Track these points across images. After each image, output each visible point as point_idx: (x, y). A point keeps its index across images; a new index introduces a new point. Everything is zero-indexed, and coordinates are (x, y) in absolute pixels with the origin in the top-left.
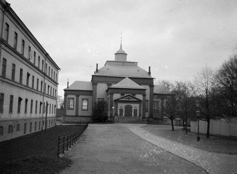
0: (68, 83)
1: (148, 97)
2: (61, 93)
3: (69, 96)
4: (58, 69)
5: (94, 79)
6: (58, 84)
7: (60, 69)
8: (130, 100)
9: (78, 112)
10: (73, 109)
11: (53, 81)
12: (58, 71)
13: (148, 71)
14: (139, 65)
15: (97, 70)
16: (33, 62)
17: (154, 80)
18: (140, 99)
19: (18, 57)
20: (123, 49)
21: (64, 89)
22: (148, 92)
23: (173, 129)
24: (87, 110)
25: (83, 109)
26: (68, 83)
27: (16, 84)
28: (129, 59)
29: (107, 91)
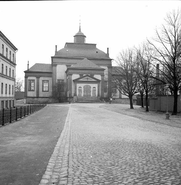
0: (28, 65)
1: (106, 77)
2: (20, 76)
3: (29, 78)
4: (15, 49)
5: (53, 61)
6: (16, 65)
7: (17, 49)
8: (89, 80)
9: (177, 104)
10: (34, 91)
11: (10, 61)
12: (16, 51)
13: (106, 53)
14: (97, 47)
15: (56, 52)
16: (5, 56)
17: (112, 61)
18: (98, 79)
19: (7, 61)
20: (82, 31)
21: (24, 71)
22: (106, 72)
23: (132, 107)
24: (48, 91)
25: (47, 90)
26: (28, 65)
27: (4, 76)
28: (88, 41)
29: (66, 72)
